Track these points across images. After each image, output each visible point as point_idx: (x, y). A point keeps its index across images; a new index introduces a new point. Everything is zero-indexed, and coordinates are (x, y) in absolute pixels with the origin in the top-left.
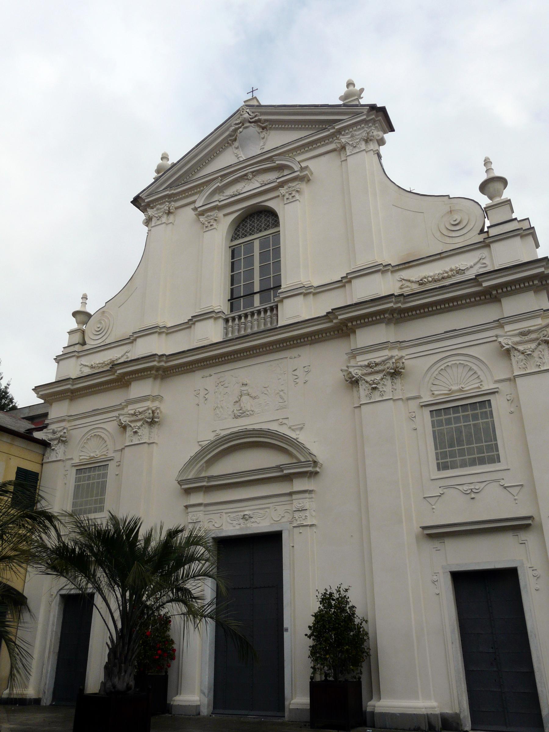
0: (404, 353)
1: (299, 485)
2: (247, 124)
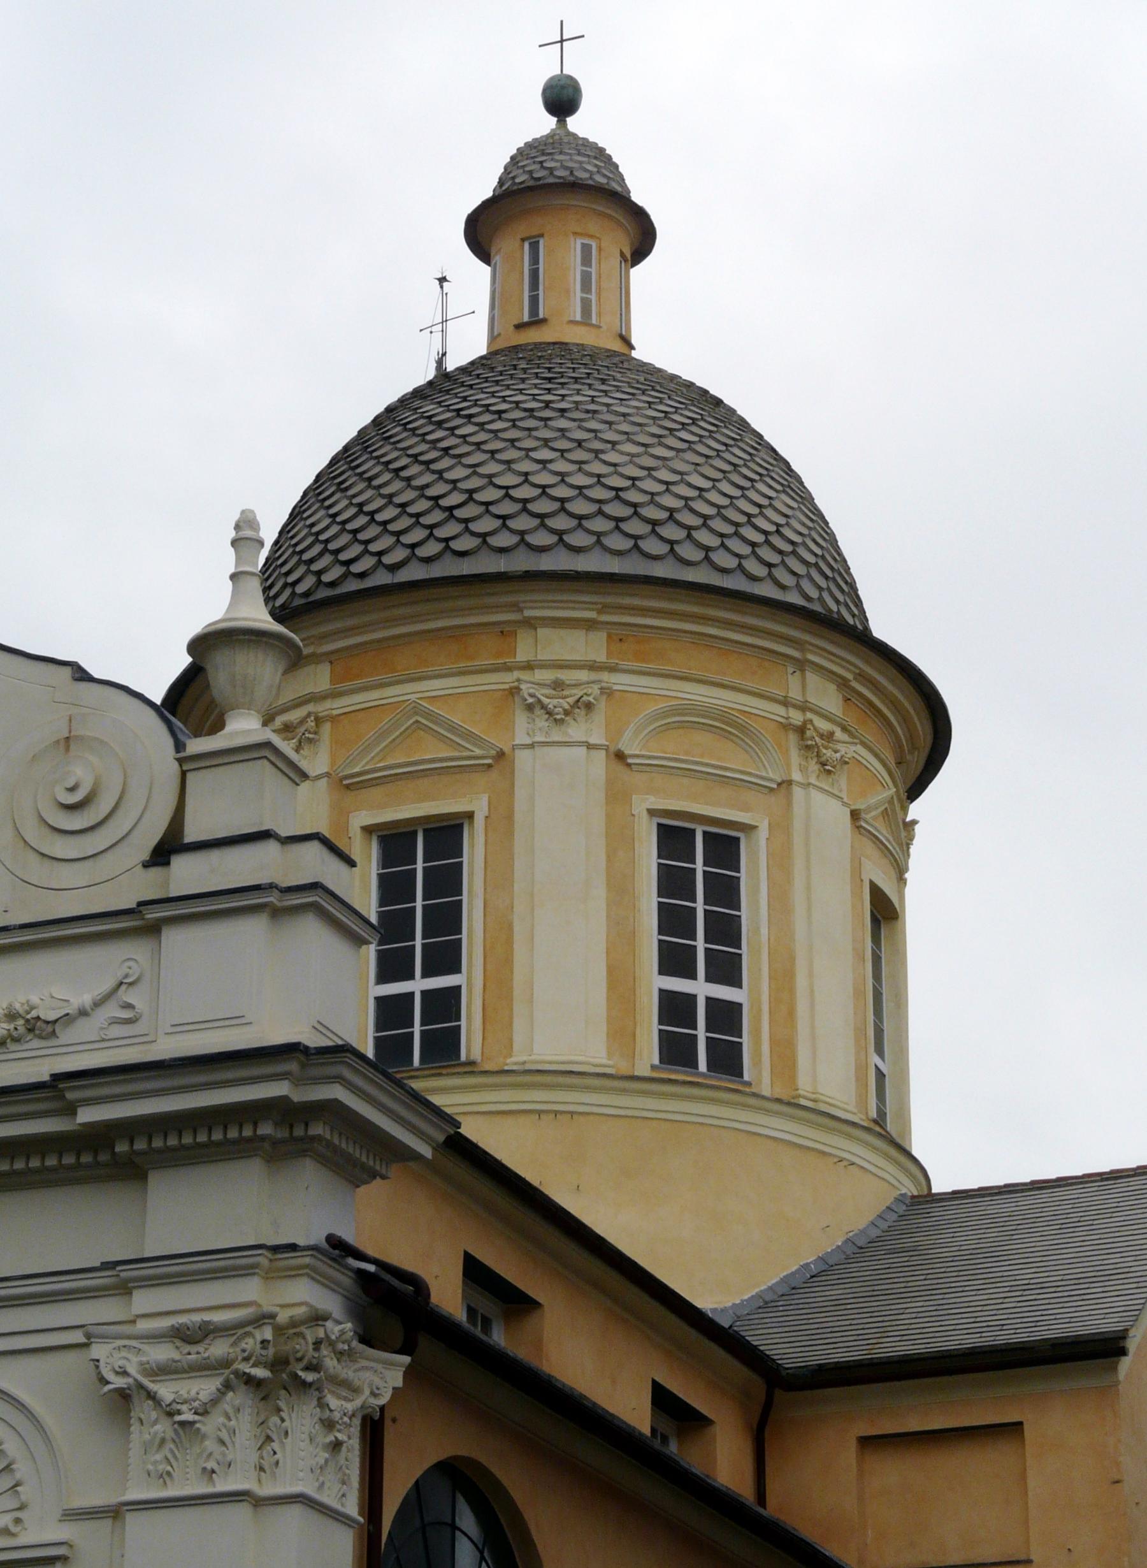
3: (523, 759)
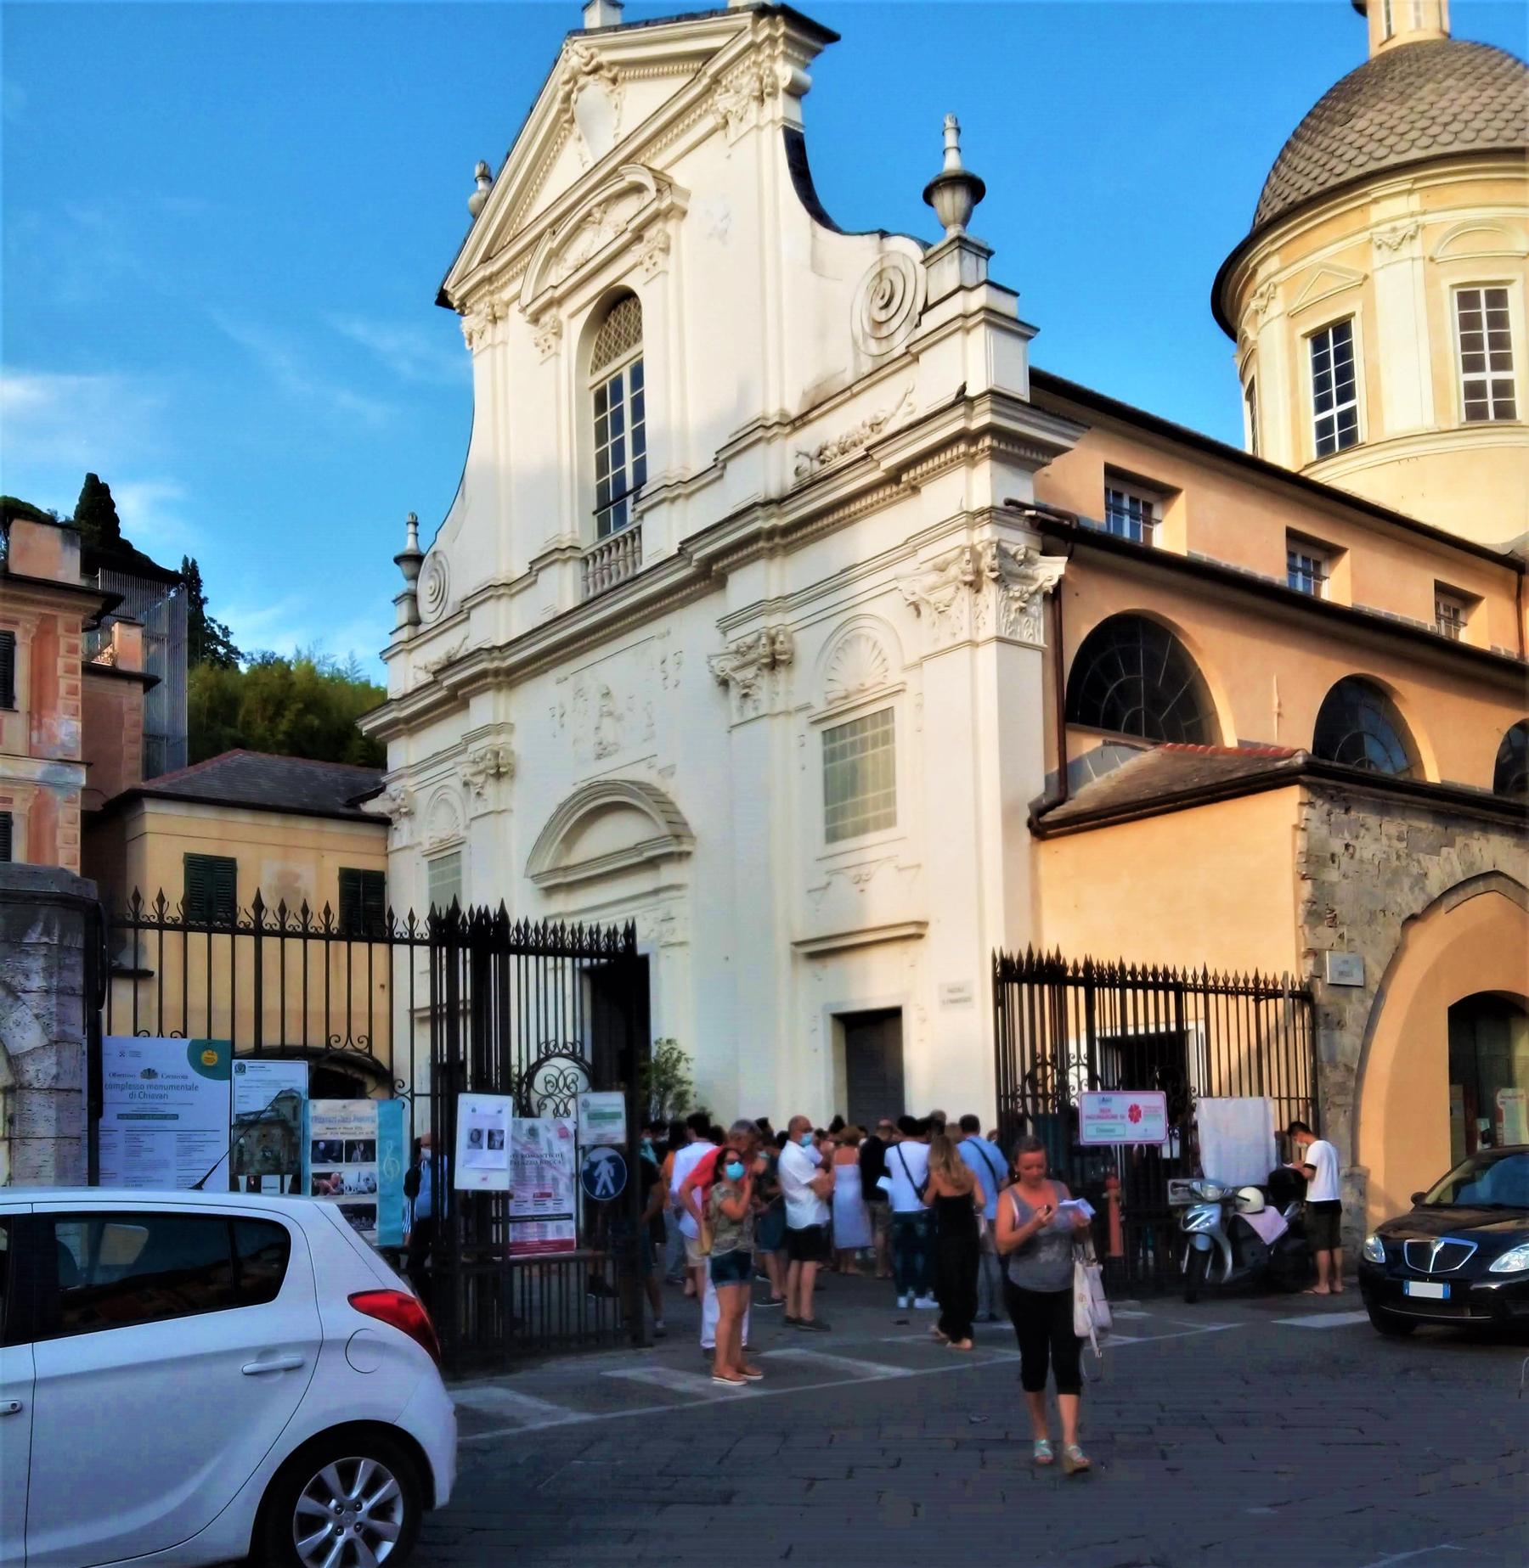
0: (789, 618)
1: (669, 874)
2: (582, 80)
3: (1379, 278)
